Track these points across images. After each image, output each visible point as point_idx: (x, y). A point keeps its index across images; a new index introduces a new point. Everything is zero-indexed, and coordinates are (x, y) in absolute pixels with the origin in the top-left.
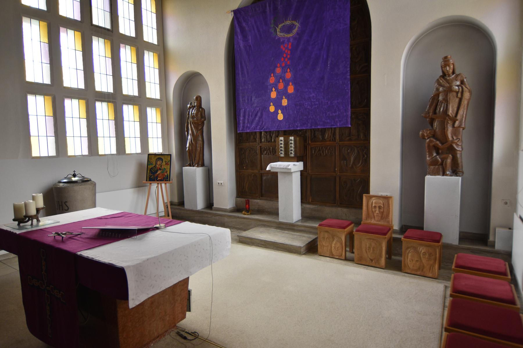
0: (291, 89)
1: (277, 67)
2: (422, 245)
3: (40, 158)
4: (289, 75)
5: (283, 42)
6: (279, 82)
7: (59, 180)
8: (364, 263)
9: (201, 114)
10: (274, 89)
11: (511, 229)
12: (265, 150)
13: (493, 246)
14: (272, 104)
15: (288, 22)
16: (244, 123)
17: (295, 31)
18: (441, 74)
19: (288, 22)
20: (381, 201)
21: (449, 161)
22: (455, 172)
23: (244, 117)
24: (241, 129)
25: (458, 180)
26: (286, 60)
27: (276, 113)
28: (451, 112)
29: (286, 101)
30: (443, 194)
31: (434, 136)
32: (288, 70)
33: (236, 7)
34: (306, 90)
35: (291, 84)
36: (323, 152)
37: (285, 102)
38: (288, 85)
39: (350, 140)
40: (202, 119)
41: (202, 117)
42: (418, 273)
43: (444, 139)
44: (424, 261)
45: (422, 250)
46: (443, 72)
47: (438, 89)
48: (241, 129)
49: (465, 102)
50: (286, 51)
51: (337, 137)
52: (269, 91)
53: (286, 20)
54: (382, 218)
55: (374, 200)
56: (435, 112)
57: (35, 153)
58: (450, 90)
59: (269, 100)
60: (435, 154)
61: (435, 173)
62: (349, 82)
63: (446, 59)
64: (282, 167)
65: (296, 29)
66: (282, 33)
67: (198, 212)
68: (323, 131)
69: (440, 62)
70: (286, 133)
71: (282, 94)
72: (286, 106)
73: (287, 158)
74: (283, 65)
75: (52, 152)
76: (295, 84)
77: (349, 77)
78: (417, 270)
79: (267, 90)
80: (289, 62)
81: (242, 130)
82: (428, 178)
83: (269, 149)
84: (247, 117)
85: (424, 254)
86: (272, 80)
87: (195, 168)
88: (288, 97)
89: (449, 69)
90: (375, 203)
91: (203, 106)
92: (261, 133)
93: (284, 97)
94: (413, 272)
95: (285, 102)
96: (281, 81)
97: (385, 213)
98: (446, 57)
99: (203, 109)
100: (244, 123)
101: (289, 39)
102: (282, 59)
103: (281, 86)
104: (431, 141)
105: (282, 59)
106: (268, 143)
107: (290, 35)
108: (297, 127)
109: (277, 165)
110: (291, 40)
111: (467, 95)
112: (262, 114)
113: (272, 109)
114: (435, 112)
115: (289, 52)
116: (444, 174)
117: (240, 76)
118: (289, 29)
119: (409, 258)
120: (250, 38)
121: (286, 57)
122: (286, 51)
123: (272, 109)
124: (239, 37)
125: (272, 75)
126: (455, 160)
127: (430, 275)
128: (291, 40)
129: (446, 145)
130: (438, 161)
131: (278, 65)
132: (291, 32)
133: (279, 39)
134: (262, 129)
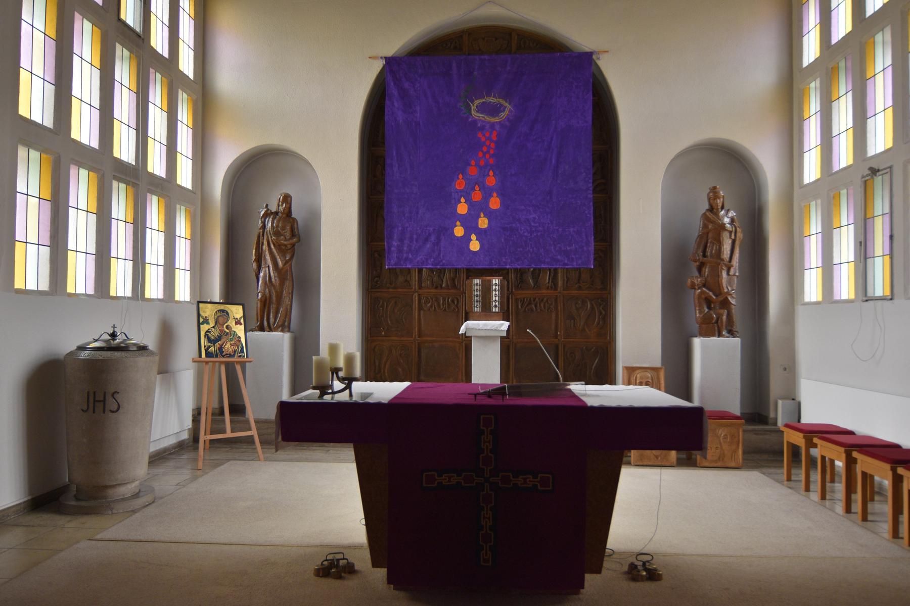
0: (495, 203)
1: (469, 164)
2: (722, 425)
3: (76, 295)
4: (491, 180)
5: (482, 128)
6: (473, 189)
7: (80, 342)
8: (645, 463)
9: (292, 230)
10: (463, 200)
12: (427, 302)
13: (775, 424)
14: (458, 223)
15: (492, 100)
16: (400, 251)
17: (504, 115)
18: (707, 207)
19: (492, 100)
21: (724, 317)
22: (731, 333)
23: (401, 240)
24: (392, 262)
25: (736, 342)
26: (487, 156)
27: (466, 239)
29: (486, 221)
30: (716, 364)
31: (704, 285)
32: (491, 173)
33: (390, 52)
34: (523, 207)
35: (495, 195)
36: (536, 306)
37: (483, 223)
38: (491, 196)
39: (580, 288)
40: (293, 238)
41: (293, 235)
42: (719, 464)
44: (725, 447)
46: (710, 205)
47: (705, 226)
48: (392, 262)
49: (737, 243)
50: (488, 143)
51: (560, 283)
52: (453, 202)
53: (489, 95)
56: (704, 256)
57: (18, 284)
59: (455, 216)
60: (707, 310)
61: (705, 333)
62: (591, 204)
63: (714, 190)
64: (489, 328)
65: (507, 112)
66: (482, 113)
72: (485, 229)
73: (487, 313)
74: (482, 163)
75: (44, 286)
76: (503, 195)
77: (591, 196)
78: (716, 462)
79: (450, 201)
80: (492, 161)
81: (396, 264)
83: (437, 300)
84: (407, 242)
85: (725, 437)
86: (460, 184)
87: (266, 333)
88: (490, 214)
90: (641, 378)
91: (295, 214)
92: (420, 270)
93: (482, 215)
94: (711, 465)
95: (483, 223)
96: (477, 188)
98: (715, 188)
99: (294, 219)
100: (400, 251)
101: (493, 125)
102: (481, 154)
103: (477, 196)
104: (702, 292)
105: (481, 154)
106: (433, 291)
107: (496, 120)
108: (506, 263)
109: (479, 325)
110: (497, 127)
111: (740, 235)
113: (459, 231)
114: (704, 256)
115: (493, 145)
116: (720, 335)
117: (395, 169)
118: (494, 110)
120: (418, 108)
121: (488, 152)
122: (488, 143)
123: (459, 231)
124: (396, 104)
125: (461, 176)
126: (729, 315)
127: (733, 464)
128: (497, 127)
129: (721, 298)
130: (712, 318)
131: (473, 162)
132: (497, 115)
133: (475, 122)
134: (438, 264)
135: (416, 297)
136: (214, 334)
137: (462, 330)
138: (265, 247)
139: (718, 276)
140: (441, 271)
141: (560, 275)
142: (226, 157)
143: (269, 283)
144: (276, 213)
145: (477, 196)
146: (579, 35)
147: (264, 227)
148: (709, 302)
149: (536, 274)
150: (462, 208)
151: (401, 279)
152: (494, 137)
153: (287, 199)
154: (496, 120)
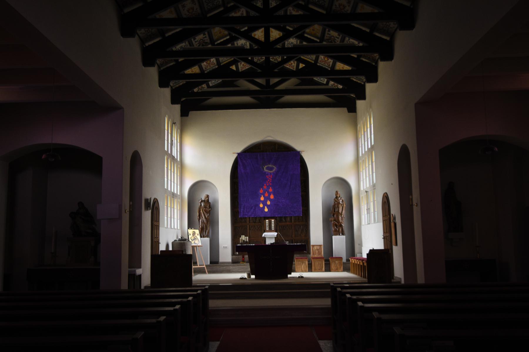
0: (272, 197)
4: (271, 190)
5: (268, 174)
11: (361, 253)
15: (270, 166)
17: (274, 170)
19: (270, 166)
20: (318, 247)
22: (343, 234)
25: (344, 237)
27: (264, 208)
28: (340, 211)
30: (339, 242)
31: (335, 220)
33: (239, 151)
37: (269, 203)
43: (338, 222)
45: (337, 262)
49: (344, 208)
54: (319, 254)
55: (315, 247)
58: (339, 203)
59: (260, 201)
63: (337, 192)
67: (420, 286)
68: (285, 218)
69: (334, 193)
70: (269, 218)
71: (266, 199)
73: (270, 230)
76: (274, 194)
82: (334, 237)
86: (261, 191)
88: (270, 200)
89: (338, 196)
91: (210, 201)
92: (249, 218)
95: (269, 203)
97: (320, 253)
99: (210, 203)
101: (271, 173)
103: (267, 195)
107: (272, 172)
111: (345, 205)
112: (255, 209)
113: (261, 206)
116: (339, 235)
118: (271, 169)
119: (333, 266)
123: (261, 206)
133: (265, 172)
135: (248, 226)
136: (193, 238)
137: (263, 236)
138: (201, 211)
139: (338, 218)
140: (256, 218)
141: (293, 218)
142: (188, 184)
143: (203, 222)
144: (204, 201)
145: (267, 195)
146: (298, 148)
147: (201, 205)
148: (336, 225)
149: (285, 218)
150: (262, 199)
151: (243, 220)
152: (271, 177)
153: (208, 196)
154: (272, 172)
